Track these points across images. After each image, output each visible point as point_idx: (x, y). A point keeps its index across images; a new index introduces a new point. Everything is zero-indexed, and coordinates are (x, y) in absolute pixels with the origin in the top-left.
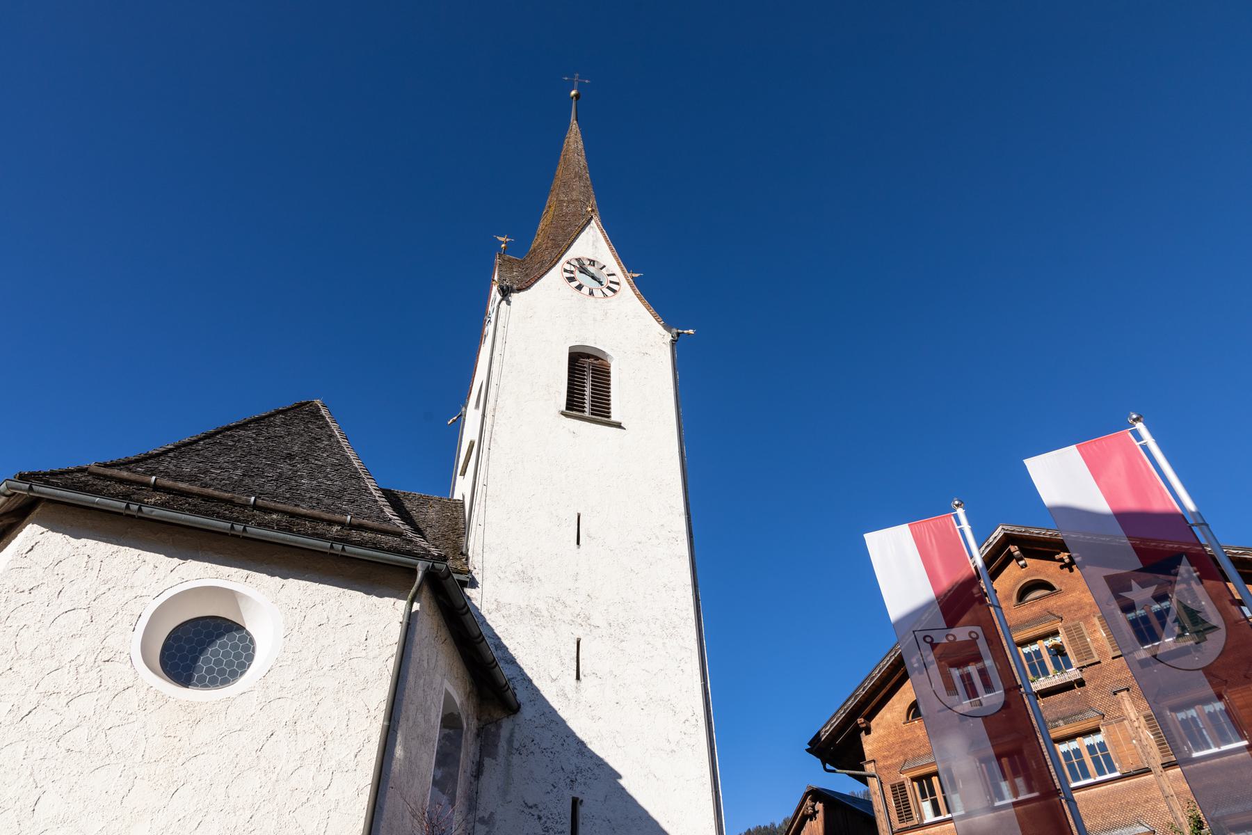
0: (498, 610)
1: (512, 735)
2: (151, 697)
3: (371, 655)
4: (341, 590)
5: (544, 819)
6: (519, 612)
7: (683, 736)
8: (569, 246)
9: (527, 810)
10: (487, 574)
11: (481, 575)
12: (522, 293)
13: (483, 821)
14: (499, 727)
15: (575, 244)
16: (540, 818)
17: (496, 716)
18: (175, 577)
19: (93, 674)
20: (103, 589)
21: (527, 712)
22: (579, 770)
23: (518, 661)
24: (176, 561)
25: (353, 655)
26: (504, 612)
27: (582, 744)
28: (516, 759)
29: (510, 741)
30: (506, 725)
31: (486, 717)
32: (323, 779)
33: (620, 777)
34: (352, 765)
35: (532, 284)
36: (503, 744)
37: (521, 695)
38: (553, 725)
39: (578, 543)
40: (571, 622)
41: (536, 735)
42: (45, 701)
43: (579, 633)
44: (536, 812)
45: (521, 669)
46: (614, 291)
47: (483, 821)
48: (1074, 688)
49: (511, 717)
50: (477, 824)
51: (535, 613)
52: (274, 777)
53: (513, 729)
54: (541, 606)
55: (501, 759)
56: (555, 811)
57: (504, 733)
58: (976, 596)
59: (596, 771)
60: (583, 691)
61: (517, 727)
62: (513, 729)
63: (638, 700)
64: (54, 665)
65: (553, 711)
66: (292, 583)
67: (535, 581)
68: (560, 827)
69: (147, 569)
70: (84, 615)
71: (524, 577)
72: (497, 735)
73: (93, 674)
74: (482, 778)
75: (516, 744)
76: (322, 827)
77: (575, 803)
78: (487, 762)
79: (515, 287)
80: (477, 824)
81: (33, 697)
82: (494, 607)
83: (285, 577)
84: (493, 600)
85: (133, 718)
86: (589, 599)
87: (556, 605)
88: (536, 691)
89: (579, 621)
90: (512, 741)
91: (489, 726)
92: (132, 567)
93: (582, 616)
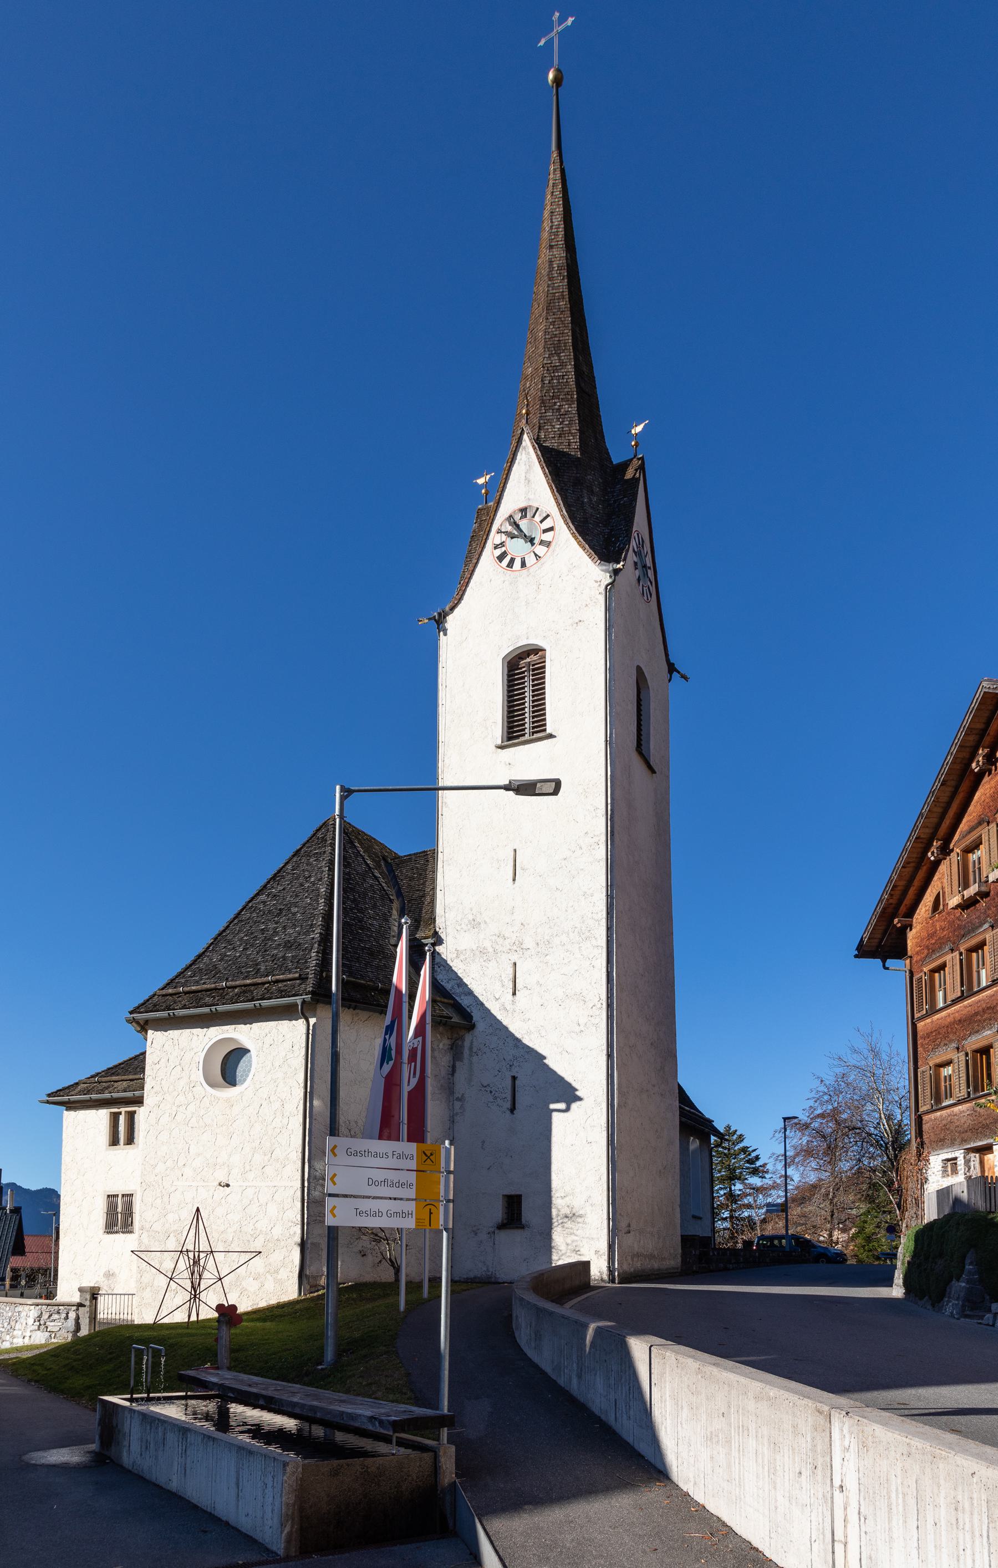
0: (457, 957)
1: (472, 1043)
2: (213, 1099)
3: (296, 1055)
4: (277, 1022)
5: (494, 1092)
6: (472, 954)
7: (590, 1018)
8: (498, 503)
9: (483, 1089)
10: (449, 930)
11: (444, 933)
12: (457, 611)
13: (458, 1099)
14: (463, 1040)
15: (505, 494)
16: (491, 1092)
17: (461, 1034)
18: (206, 1039)
19: (190, 1094)
20: (182, 1054)
21: (481, 1026)
22: (515, 1058)
23: (475, 993)
24: (205, 1029)
25: (288, 1058)
26: (462, 957)
27: (518, 1041)
28: (475, 1059)
29: (471, 1049)
30: (468, 1038)
31: (456, 1035)
32: (285, 1121)
33: (545, 1058)
34: (296, 1112)
35: (465, 591)
36: (466, 1052)
37: (476, 1016)
38: (497, 1032)
39: (514, 880)
40: (509, 951)
41: (487, 1041)
42: (178, 1109)
43: (514, 958)
44: (488, 1089)
45: (476, 997)
46: (551, 529)
47: (458, 1099)
48: (979, 902)
49: (471, 1032)
50: (455, 1101)
51: (483, 952)
52: (265, 1124)
53: (472, 1040)
54: (487, 944)
55: (466, 1061)
56: (500, 1086)
57: (467, 1044)
58: (976, 770)
59: (526, 1056)
60: (517, 1002)
61: (475, 1038)
62: (472, 1040)
63: (557, 999)
64: (177, 1093)
65: (499, 1022)
66: (255, 1025)
67: (483, 925)
68: (504, 1096)
69: (195, 1038)
70: (179, 1068)
71: (475, 924)
72: (462, 1046)
73: (190, 1094)
74: (456, 1075)
75: (475, 1049)
76: (288, 1142)
77: (514, 1078)
78: (458, 1064)
79: (447, 609)
80: (455, 1101)
81: (174, 1108)
82: (455, 955)
83: (251, 1024)
84: (454, 950)
85: (209, 1110)
86: (522, 926)
87: (498, 940)
88: (487, 1011)
89: (515, 948)
90: (472, 1048)
91: (457, 1042)
92: (190, 1039)
93: (517, 943)
